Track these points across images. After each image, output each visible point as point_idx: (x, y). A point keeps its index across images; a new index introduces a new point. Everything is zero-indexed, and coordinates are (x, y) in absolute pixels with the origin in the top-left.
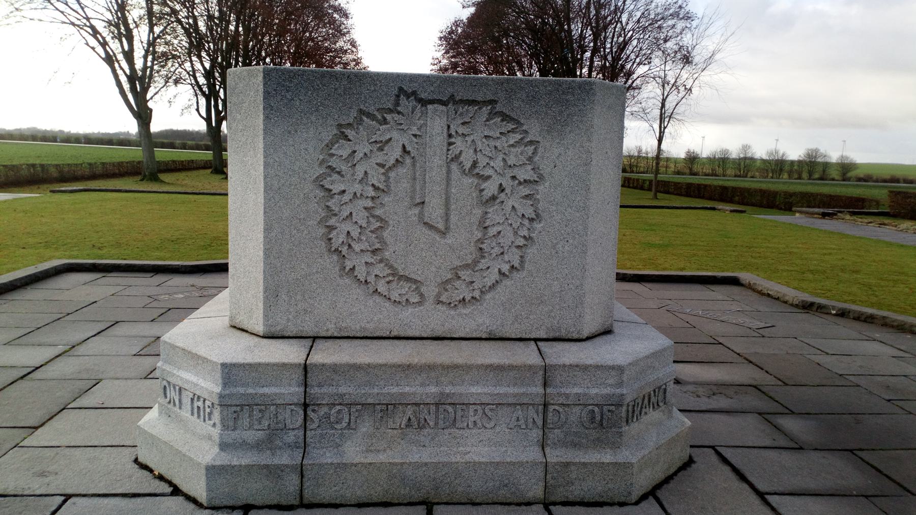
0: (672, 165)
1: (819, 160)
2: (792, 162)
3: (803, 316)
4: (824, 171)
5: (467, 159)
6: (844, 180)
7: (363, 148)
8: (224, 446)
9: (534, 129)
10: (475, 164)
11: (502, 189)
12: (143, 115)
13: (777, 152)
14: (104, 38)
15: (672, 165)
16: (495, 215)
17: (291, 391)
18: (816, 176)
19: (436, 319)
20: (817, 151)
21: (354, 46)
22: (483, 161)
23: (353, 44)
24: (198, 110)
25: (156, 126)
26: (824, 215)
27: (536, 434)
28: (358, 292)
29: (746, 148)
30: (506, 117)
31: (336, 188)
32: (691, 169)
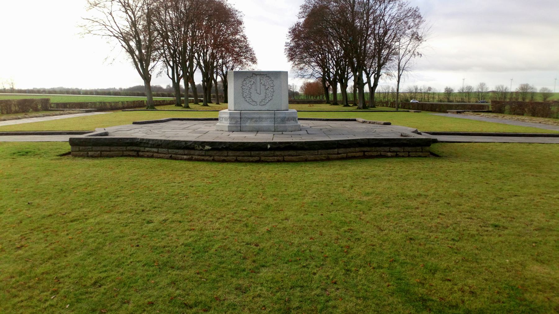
0: (437, 97)
1: (529, 91)
2: (512, 93)
3: (364, 124)
4: (532, 97)
9: (273, 78)
12: (146, 77)
13: (502, 87)
15: (437, 97)
16: (267, 91)
17: (239, 116)
19: (259, 108)
20: (527, 85)
21: (245, 39)
23: (244, 37)
24: (168, 74)
25: (153, 83)
26: (458, 112)
28: (247, 103)
29: (482, 85)
32: (448, 99)
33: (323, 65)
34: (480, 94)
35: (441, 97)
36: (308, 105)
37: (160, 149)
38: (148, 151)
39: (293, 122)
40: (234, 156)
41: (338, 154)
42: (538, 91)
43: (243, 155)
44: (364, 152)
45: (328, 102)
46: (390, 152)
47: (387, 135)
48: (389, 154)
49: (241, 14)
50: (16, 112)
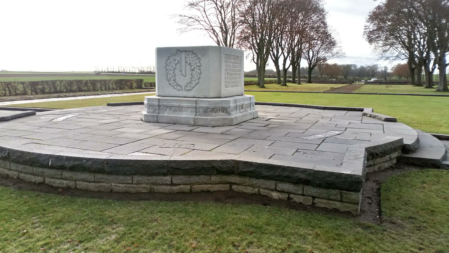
5: (188, 62)
7: (172, 61)
8: (148, 112)
10: (190, 63)
11: (195, 68)
14: (217, 34)
17: (157, 103)
19: (185, 93)
22: (191, 62)
27: (194, 113)
30: (195, 54)
33: (409, 47)
36: (386, 85)
39: (221, 113)
40: (16, 171)
41: (172, 184)
43: (26, 171)
44: (231, 184)
45: (413, 83)
46: (276, 190)
48: (275, 195)
49: (323, 3)
50: (113, 89)
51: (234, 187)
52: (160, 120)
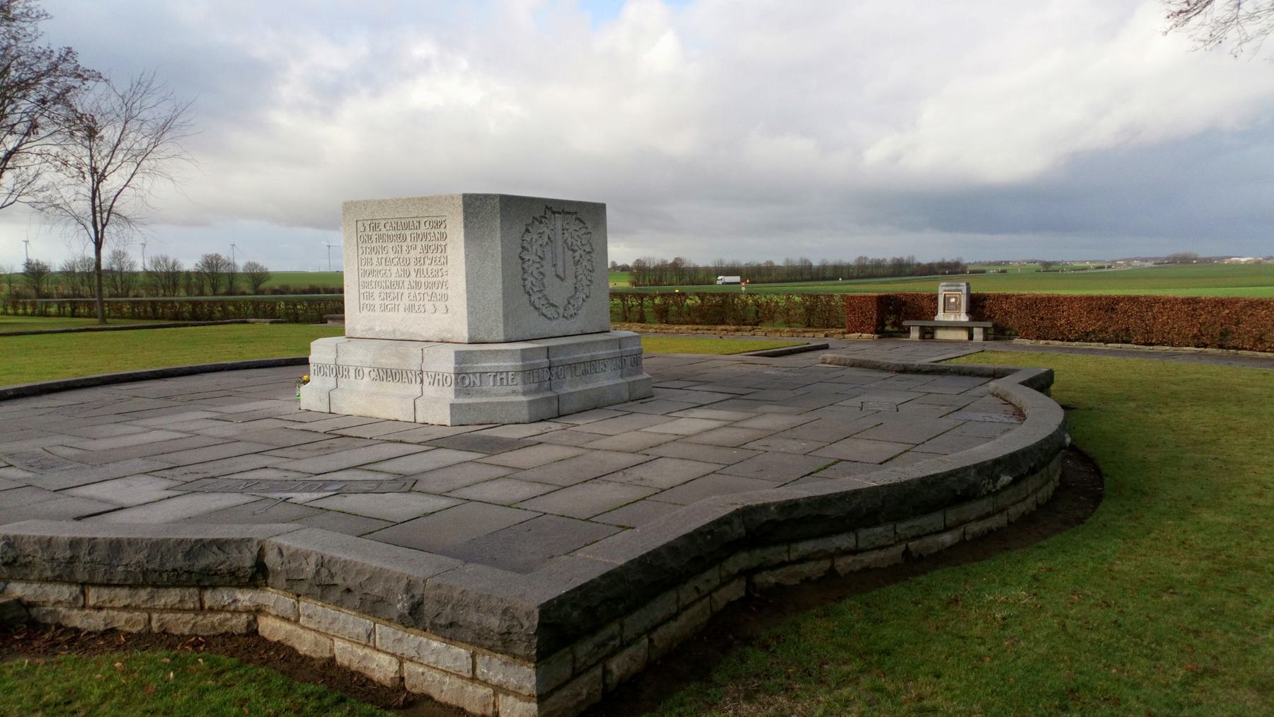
1: (223, 270)
2: (188, 274)
4: (231, 283)
6: (257, 293)
7: (535, 237)
9: (589, 225)
13: (165, 260)
18: (223, 290)
20: (217, 257)
31: (526, 258)
32: (38, 290)
34: (118, 279)
35: (18, 287)
37: (863, 533)
38: (803, 560)
42: (240, 270)
47: (58, 403)
51: (759, 579)
52: (566, 408)
